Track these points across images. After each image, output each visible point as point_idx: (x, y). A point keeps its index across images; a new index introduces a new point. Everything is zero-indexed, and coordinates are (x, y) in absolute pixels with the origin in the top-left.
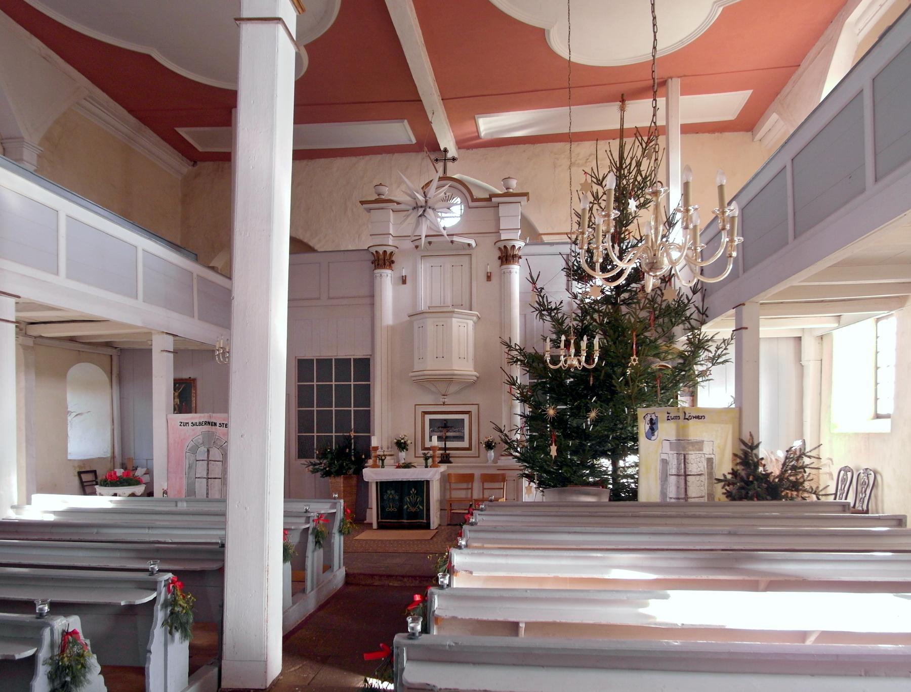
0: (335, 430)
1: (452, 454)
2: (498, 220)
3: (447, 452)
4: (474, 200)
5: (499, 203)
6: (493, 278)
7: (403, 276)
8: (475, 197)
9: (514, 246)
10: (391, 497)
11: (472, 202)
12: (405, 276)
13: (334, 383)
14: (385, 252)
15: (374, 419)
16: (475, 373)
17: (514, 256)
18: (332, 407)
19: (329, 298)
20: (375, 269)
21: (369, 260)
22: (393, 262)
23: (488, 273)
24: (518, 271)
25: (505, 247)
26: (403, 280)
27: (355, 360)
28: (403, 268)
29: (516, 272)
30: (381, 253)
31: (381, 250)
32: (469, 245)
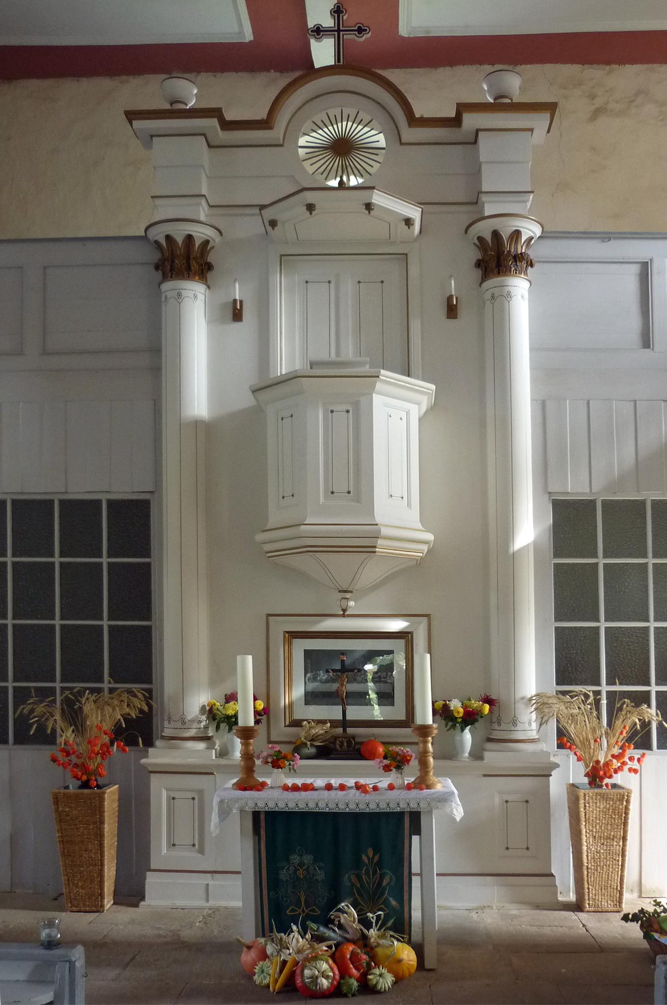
0: (62, 675)
1: (360, 736)
2: (475, 173)
3: (350, 731)
4: (413, 121)
5: (477, 131)
6: (462, 312)
7: (235, 301)
8: (417, 115)
9: (517, 234)
10: (301, 873)
11: (410, 125)
12: (241, 302)
13: (57, 622)
14: (189, 238)
15: (161, 640)
16: (430, 537)
17: (519, 258)
18: (55, 688)
19: (45, 352)
20: (165, 278)
21: (149, 264)
22: (210, 267)
23: (450, 298)
24: (526, 296)
25: (496, 234)
26: (235, 308)
27: (110, 503)
28: (235, 281)
29: (523, 297)
30: (180, 240)
31: (179, 232)
32: (408, 222)
